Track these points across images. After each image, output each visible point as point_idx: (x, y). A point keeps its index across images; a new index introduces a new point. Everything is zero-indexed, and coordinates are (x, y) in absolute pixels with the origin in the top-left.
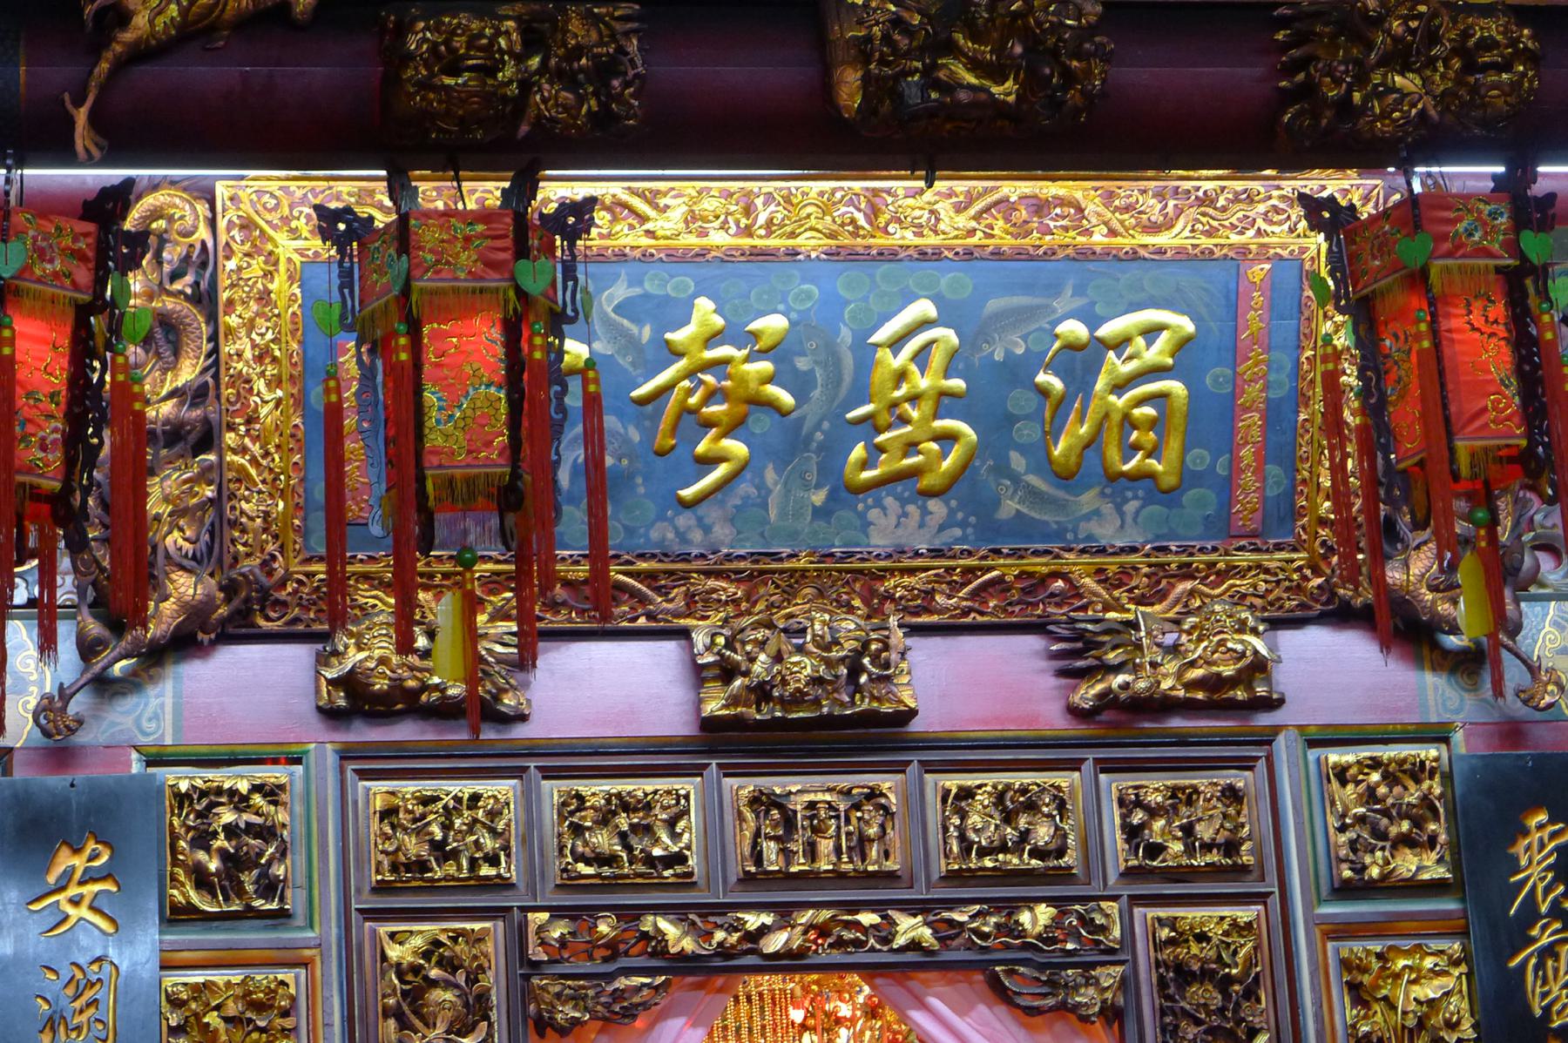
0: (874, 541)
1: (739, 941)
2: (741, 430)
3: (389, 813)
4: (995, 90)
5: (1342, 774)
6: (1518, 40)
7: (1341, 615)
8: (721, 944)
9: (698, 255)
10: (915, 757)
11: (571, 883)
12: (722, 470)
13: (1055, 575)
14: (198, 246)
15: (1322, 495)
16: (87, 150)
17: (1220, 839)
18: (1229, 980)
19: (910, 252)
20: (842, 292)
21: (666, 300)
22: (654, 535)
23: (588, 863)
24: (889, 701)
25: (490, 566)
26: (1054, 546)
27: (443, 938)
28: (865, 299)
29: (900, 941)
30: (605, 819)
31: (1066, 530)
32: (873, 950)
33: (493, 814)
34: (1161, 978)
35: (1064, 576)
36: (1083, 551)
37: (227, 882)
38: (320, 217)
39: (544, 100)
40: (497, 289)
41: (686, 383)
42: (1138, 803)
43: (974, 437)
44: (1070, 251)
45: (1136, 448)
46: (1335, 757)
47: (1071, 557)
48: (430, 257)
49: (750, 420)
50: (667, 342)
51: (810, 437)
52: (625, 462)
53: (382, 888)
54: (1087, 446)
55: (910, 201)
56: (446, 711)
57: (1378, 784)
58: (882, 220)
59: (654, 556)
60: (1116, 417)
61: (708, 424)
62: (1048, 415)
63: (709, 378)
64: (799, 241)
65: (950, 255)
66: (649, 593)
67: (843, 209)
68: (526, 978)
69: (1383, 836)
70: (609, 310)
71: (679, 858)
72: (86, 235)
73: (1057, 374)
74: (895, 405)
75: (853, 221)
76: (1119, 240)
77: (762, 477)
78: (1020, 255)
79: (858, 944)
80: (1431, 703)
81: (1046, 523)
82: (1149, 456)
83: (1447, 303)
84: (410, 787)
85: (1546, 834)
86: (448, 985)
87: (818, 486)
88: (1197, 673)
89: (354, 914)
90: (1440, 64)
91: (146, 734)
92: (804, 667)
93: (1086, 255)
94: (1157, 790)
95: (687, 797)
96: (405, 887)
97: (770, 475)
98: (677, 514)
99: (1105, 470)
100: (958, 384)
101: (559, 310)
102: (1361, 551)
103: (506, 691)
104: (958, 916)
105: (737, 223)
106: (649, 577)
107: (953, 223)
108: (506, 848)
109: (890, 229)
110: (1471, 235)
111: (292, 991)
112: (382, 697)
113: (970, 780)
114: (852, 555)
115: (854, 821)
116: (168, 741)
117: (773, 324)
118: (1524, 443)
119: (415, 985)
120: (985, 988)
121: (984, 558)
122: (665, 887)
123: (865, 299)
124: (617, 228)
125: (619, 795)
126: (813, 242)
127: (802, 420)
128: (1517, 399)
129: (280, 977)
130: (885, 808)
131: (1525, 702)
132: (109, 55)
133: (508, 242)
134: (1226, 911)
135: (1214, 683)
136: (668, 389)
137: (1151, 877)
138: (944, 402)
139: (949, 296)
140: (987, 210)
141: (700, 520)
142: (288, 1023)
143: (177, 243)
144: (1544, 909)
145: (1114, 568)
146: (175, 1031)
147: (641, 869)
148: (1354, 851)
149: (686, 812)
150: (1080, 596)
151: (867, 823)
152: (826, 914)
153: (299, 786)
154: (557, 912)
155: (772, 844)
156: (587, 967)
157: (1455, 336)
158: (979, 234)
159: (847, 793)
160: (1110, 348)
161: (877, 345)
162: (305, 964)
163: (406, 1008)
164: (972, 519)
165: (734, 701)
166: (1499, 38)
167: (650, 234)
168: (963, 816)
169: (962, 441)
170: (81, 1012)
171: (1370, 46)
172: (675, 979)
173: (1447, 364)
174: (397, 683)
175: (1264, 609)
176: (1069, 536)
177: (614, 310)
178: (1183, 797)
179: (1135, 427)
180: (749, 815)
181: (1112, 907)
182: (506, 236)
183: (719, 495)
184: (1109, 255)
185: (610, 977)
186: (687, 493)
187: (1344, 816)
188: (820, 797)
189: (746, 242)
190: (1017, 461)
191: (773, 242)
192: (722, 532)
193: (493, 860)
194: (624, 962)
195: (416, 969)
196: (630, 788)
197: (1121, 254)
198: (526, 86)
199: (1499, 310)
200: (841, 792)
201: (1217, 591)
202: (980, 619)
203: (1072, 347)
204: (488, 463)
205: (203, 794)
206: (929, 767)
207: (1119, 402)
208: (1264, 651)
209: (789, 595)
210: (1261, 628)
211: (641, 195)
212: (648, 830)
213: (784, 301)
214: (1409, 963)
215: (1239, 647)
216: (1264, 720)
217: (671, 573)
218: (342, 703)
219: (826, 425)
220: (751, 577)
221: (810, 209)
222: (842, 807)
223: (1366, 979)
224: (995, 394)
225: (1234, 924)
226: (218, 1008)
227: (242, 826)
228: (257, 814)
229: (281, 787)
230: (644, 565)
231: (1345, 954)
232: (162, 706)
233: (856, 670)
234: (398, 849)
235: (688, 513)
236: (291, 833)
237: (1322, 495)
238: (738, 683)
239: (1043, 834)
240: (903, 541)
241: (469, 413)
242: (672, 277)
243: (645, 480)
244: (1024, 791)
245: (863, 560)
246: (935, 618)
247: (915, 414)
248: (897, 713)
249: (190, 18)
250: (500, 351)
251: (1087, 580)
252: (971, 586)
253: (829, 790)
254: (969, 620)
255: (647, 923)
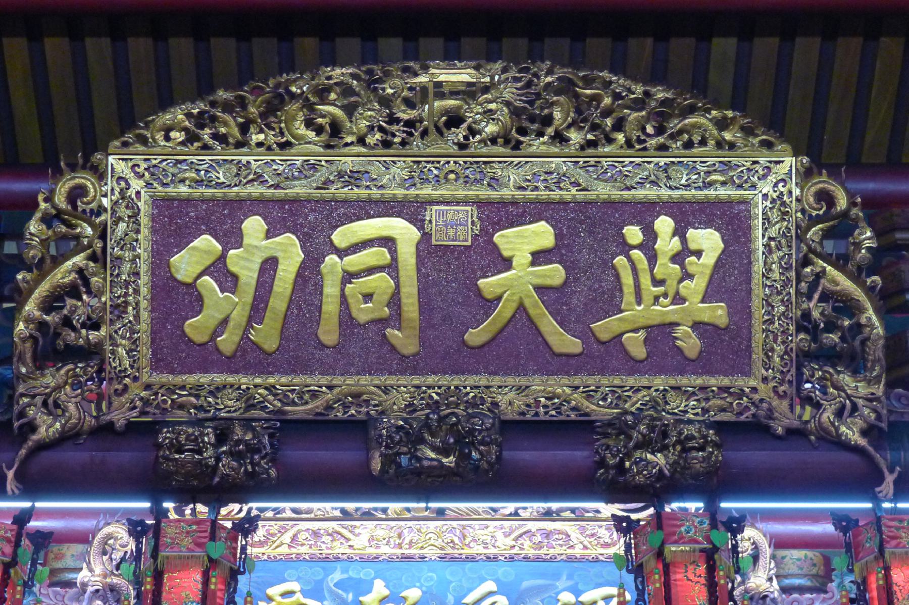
4: (444, 460)
16: (13, 491)
19: (482, 557)
20: (449, 577)
21: (360, 581)
28: (460, 581)
39: (223, 466)
40: (200, 556)
44: (564, 557)
58: (467, 541)
65: (503, 558)
67: (448, 535)
70: (332, 585)
72: (11, 531)
75: (452, 542)
78: (538, 559)
90: (671, 448)
93: (571, 559)
101: (236, 568)
107: (503, 544)
110: (688, 532)
123: (460, 581)
124: (335, 544)
132: (26, 446)
133: (207, 534)
140: (521, 536)
157: (678, 583)
158: (517, 548)
166: (696, 434)
171: (630, 438)
182: (206, 531)
189: (398, 552)
191: (413, 551)
197: (590, 558)
198: (218, 459)
199: (702, 568)
213: (419, 581)
242: (363, 568)
249: (66, 429)
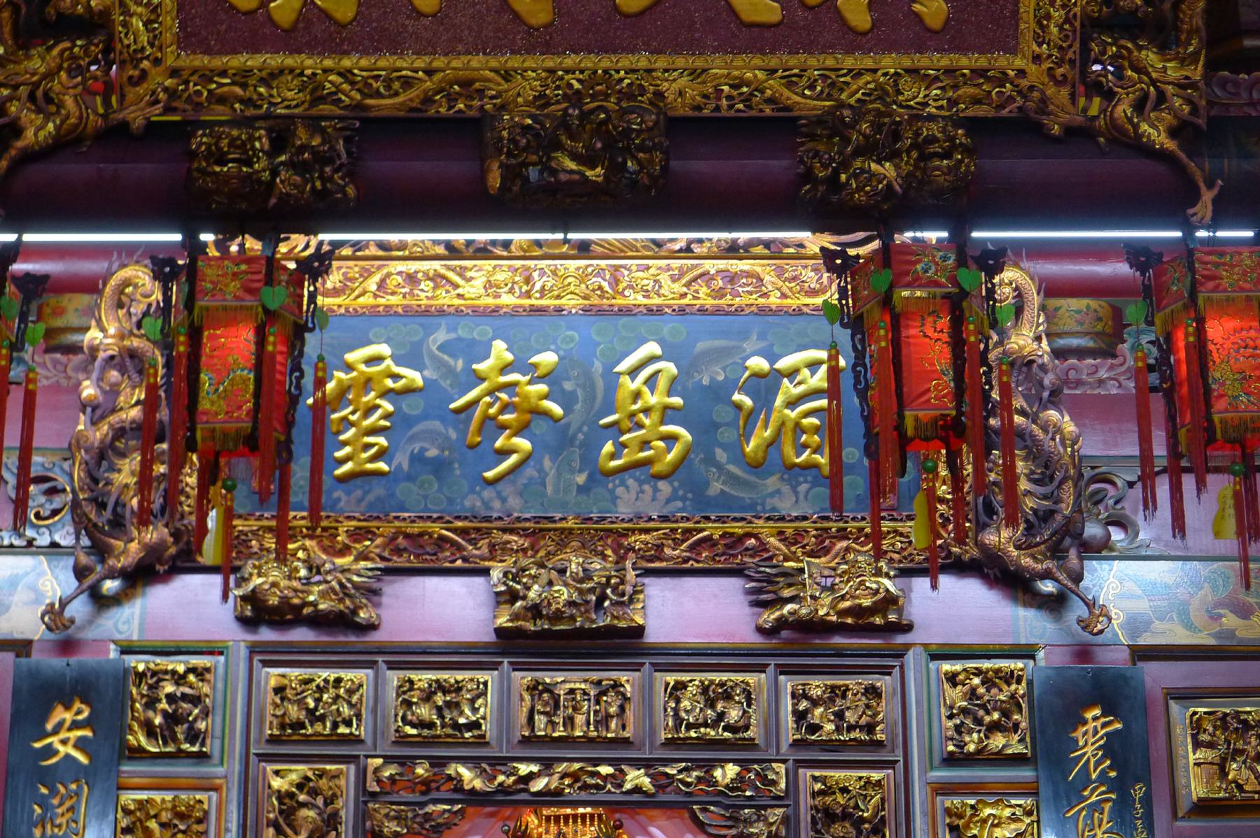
0: (620, 509)
1: (515, 782)
2: (526, 432)
3: (279, 690)
4: (589, 173)
5: (952, 679)
6: (954, 138)
7: (960, 568)
8: (501, 784)
9: (494, 311)
10: (647, 661)
11: (403, 740)
12: (514, 458)
13: (748, 535)
14: (154, 305)
15: (940, 481)
17: (863, 721)
18: (862, 820)
19: (641, 309)
20: (595, 337)
21: (472, 343)
22: (467, 503)
23: (413, 726)
24: (625, 619)
25: (354, 523)
26: (748, 515)
27: (310, 774)
28: (611, 342)
29: (628, 786)
30: (428, 697)
31: (757, 504)
32: (609, 792)
33: (351, 692)
34: (813, 817)
35: (756, 536)
36: (769, 519)
37: (167, 735)
38: (153, 263)
39: (282, 182)
40: (251, 307)
41: (487, 399)
42: (805, 696)
43: (689, 437)
44: (754, 308)
45: (805, 446)
46: (947, 667)
47: (760, 523)
48: (209, 286)
49: (532, 424)
50: (474, 371)
51: (575, 435)
52: (447, 453)
53: (273, 740)
54: (770, 445)
55: (640, 274)
56: (319, 621)
57: (977, 686)
58: (620, 288)
59: (466, 518)
60: (790, 425)
61: (503, 427)
62: (741, 423)
63: (504, 396)
64: (563, 301)
66: (464, 543)
68: (365, 803)
69: (978, 721)
70: (434, 348)
71: (475, 725)
73: (747, 395)
74: (632, 415)
75: (600, 288)
76: (789, 301)
77: (541, 464)
78: (718, 311)
79: (597, 787)
80: (1022, 630)
81: (743, 499)
82: (815, 452)
83: (908, 319)
84: (295, 673)
85: (1098, 724)
86: (314, 806)
87: (581, 471)
88: (847, 604)
89: (252, 757)
91: (120, 633)
92: (563, 593)
93: (764, 311)
94: (818, 686)
95: (485, 684)
96: (288, 740)
97: (547, 463)
98: (482, 489)
99: (784, 463)
100: (677, 401)
102: (969, 521)
103: (361, 608)
104: (669, 770)
105: (520, 288)
106: (463, 532)
108: (359, 716)
109: (626, 293)
110: (926, 271)
111: (206, 806)
112: (274, 610)
113: (685, 677)
114: (604, 519)
115: (603, 704)
116: (135, 637)
117: (547, 359)
118: (954, 413)
119: (288, 804)
120: (689, 821)
121: (698, 522)
122: (466, 744)
124: (438, 292)
125: (437, 681)
126: (573, 302)
127: (568, 425)
128: (952, 384)
129: (198, 797)
130: (623, 695)
131: (1084, 628)
134: (864, 774)
135: (857, 611)
136: (475, 402)
137: (812, 749)
138: (668, 413)
139: (669, 339)
140: (695, 280)
141: (499, 493)
142: (201, 828)
143: (140, 302)
144: (1094, 776)
145: (790, 530)
146: (126, 831)
147: (449, 731)
148: (959, 732)
149: (484, 694)
150: (767, 550)
151: (610, 704)
152: (577, 766)
153: (221, 670)
154: (388, 759)
155: (542, 717)
156: (410, 797)
158: (689, 296)
159: (599, 683)
160: (784, 376)
161: (620, 374)
162: (216, 789)
163: (281, 820)
164: (690, 495)
165: (515, 617)
167: (460, 296)
168: (678, 701)
169: (681, 441)
170: (63, 815)
172: (470, 810)
173: (904, 359)
174: (285, 600)
175: (900, 562)
176: (759, 508)
177: (438, 349)
178: (837, 693)
179: (804, 432)
180: (527, 697)
181: (781, 768)
182: (260, 272)
183: (512, 477)
184: (778, 311)
185: (422, 805)
186: (489, 474)
187: (951, 707)
188: (577, 685)
189: (526, 302)
190: (721, 455)
192: (514, 502)
193: (348, 723)
194: (435, 795)
195: (291, 795)
196: (446, 677)
200: (592, 683)
201: (865, 549)
202: (696, 565)
203: (757, 375)
204: (238, 419)
205: (154, 674)
206: (659, 668)
207: (792, 414)
208: (892, 589)
209: (562, 546)
210: (892, 573)
211: (453, 270)
212: (457, 705)
213: (555, 343)
214: (994, 812)
215: (874, 586)
216: (901, 639)
217: (478, 530)
218: (248, 613)
219: (585, 428)
220: (534, 533)
221: (570, 280)
222: (592, 693)
223: (961, 822)
224: (704, 408)
225: (868, 782)
226: (155, 816)
227: (179, 694)
228: (191, 687)
229: (208, 670)
230: (460, 524)
231: (948, 804)
232: (133, 614)
233: (602, 598)
234: (284, 714)
235: (490, 489)
236: (213, 703)
237: (940, 481)
238: (518, 604)
239: (734, 714)
240: (641, 509)
241: (229, 388)
242: (477, 326)
243: (460, 465)
244: (722, 684)
245: (612, 522)
246: (664, 564)
247: (647, 422)
248: (630, 628)
250: (253, 348)
251: (772, 540)
252: (690, 542)
253: (585, 681)
254: (688, 565)
255: (451, 770)
